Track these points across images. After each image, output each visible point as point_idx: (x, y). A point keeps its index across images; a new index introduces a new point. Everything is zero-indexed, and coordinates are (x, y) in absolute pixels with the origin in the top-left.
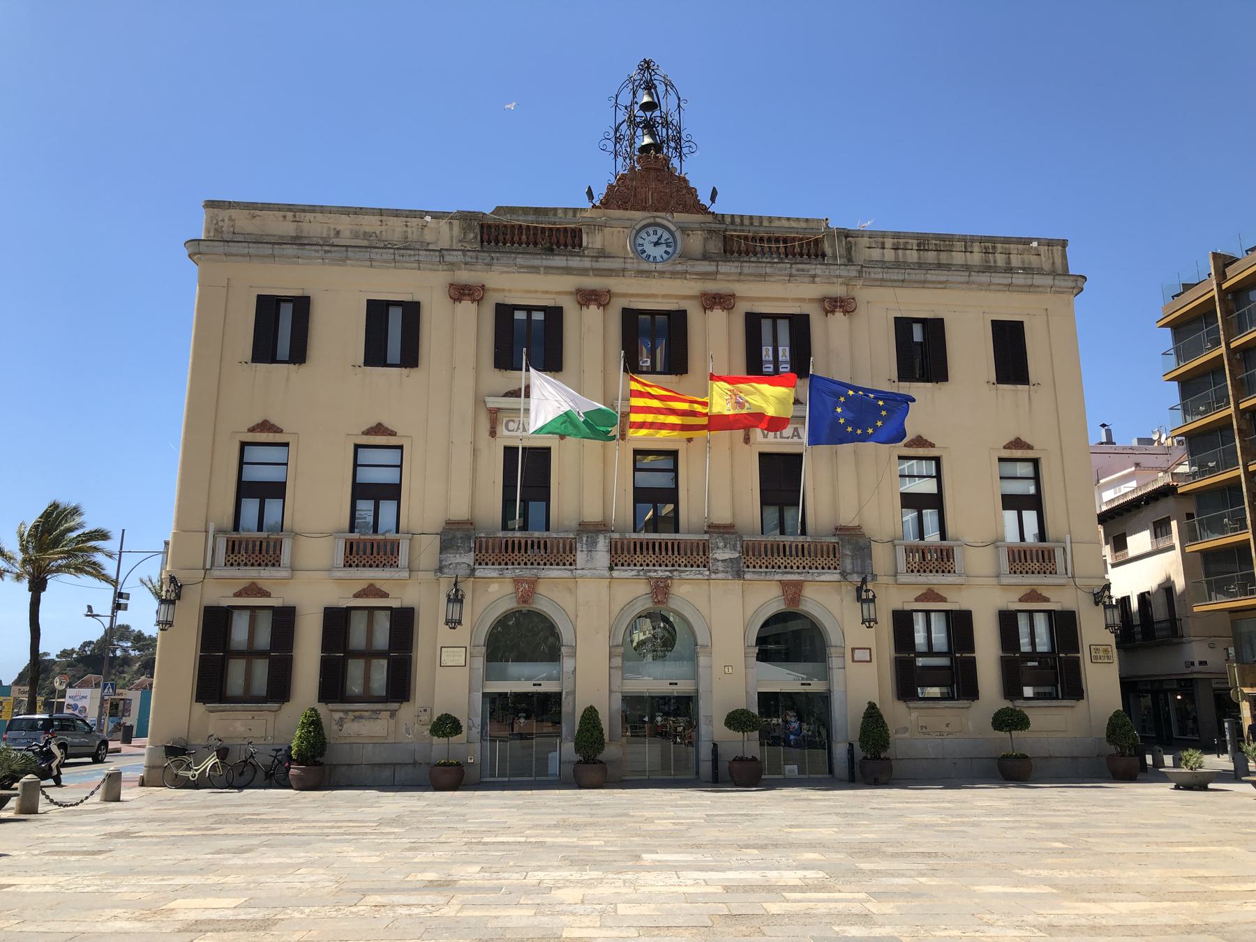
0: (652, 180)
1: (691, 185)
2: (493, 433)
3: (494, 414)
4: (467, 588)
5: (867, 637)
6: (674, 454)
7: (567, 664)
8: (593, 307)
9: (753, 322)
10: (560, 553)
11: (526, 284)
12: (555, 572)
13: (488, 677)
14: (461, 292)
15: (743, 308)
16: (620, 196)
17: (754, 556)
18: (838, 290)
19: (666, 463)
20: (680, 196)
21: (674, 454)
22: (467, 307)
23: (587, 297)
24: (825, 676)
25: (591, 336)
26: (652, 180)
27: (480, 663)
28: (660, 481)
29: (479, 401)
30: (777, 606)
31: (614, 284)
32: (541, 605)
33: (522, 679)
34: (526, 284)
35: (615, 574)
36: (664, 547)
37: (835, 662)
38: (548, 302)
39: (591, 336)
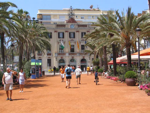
0: (72, 20)
1: (34, 14)
2: (80, 44)
3: (58, 42)
4: (57, 57)
5: (90, 61)
6: (74, 45)
7: (65, 63)
8: (67, 32)
9: (70, 33)
10: (76, 54)
11: (61, 30)
12: (75, 56)
13: (59, 64)
14: (55, 31)
15: (69, 32)
16: (69, 22)
17: (80, 54)
18: (88, 30)
19: (73, 46)
20: (75, 22)
21: (74, 45)
22: (56, 33)
23: (66, 31)
24: (86, 64)
25: (67, 35)
26: (72, 20)
27: (58, 63)
28: (73, 48)
29: (57, 41)
30: (82, 58)
31: (68, 30)
32: (85, 58)
33: (62, 64)
34: (61, 30)
35: (58, 56)
36: (73, 54)
37: (87, 63)
38: (74, 32)
39: (67, 35)
